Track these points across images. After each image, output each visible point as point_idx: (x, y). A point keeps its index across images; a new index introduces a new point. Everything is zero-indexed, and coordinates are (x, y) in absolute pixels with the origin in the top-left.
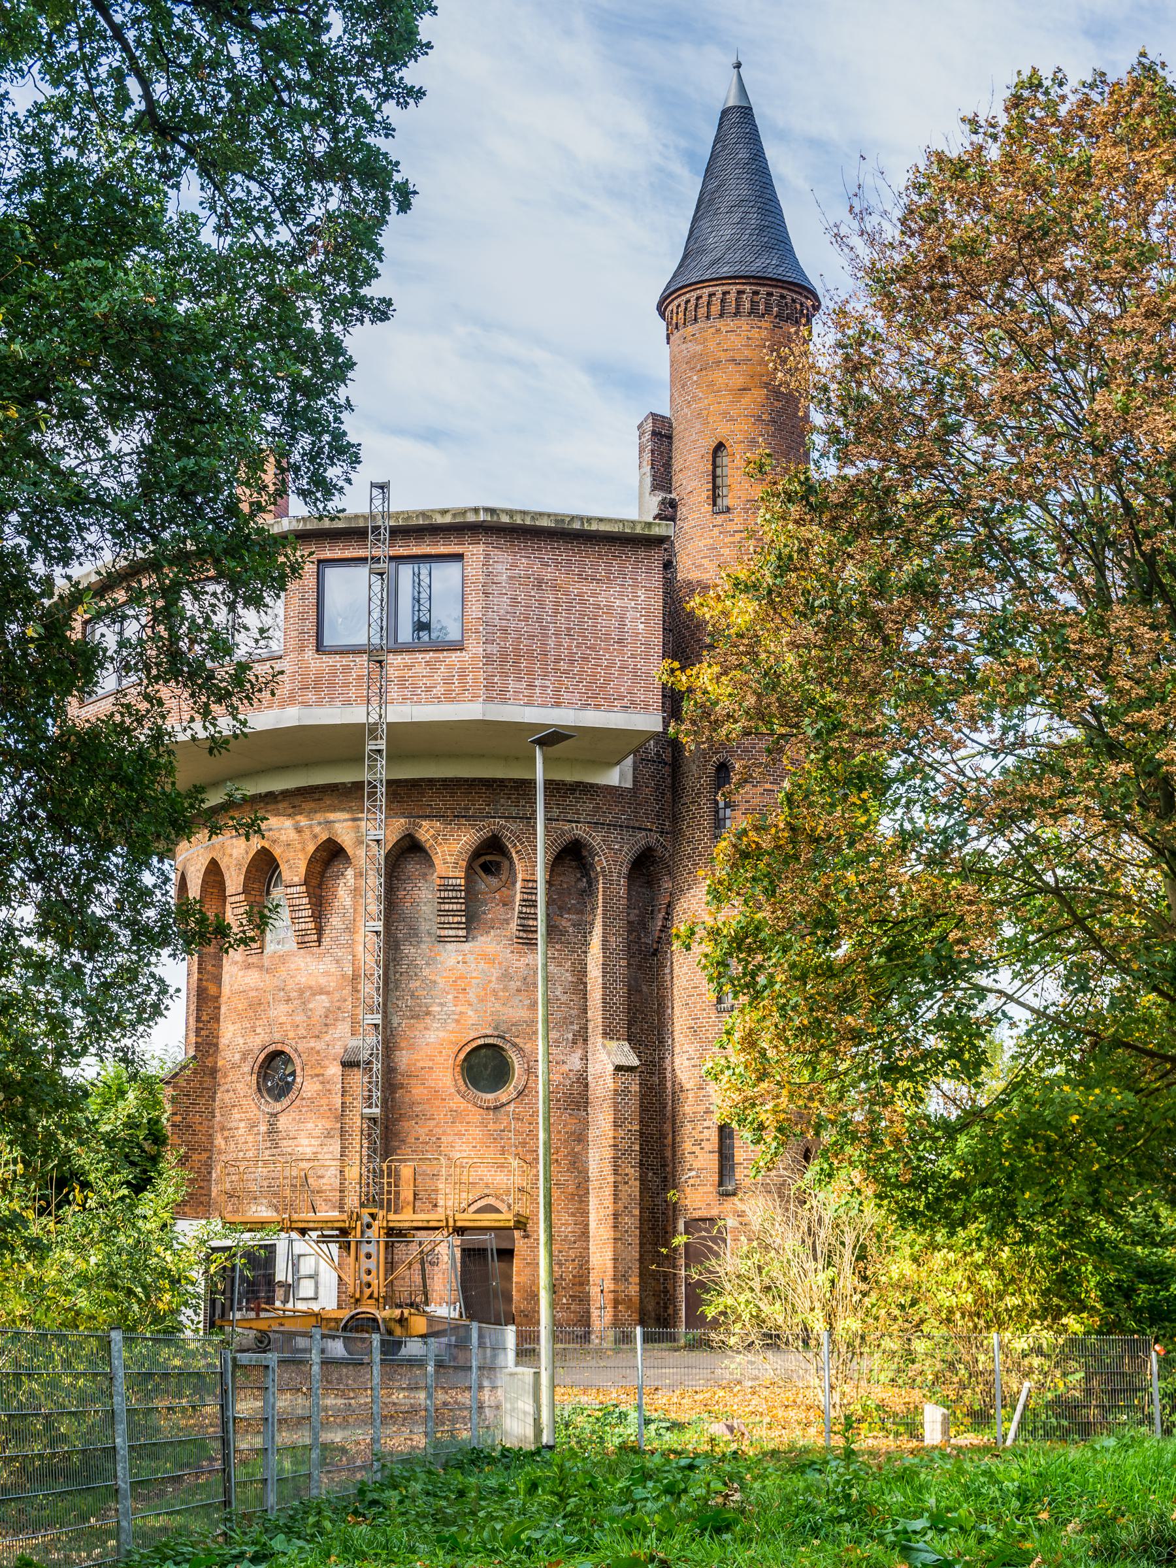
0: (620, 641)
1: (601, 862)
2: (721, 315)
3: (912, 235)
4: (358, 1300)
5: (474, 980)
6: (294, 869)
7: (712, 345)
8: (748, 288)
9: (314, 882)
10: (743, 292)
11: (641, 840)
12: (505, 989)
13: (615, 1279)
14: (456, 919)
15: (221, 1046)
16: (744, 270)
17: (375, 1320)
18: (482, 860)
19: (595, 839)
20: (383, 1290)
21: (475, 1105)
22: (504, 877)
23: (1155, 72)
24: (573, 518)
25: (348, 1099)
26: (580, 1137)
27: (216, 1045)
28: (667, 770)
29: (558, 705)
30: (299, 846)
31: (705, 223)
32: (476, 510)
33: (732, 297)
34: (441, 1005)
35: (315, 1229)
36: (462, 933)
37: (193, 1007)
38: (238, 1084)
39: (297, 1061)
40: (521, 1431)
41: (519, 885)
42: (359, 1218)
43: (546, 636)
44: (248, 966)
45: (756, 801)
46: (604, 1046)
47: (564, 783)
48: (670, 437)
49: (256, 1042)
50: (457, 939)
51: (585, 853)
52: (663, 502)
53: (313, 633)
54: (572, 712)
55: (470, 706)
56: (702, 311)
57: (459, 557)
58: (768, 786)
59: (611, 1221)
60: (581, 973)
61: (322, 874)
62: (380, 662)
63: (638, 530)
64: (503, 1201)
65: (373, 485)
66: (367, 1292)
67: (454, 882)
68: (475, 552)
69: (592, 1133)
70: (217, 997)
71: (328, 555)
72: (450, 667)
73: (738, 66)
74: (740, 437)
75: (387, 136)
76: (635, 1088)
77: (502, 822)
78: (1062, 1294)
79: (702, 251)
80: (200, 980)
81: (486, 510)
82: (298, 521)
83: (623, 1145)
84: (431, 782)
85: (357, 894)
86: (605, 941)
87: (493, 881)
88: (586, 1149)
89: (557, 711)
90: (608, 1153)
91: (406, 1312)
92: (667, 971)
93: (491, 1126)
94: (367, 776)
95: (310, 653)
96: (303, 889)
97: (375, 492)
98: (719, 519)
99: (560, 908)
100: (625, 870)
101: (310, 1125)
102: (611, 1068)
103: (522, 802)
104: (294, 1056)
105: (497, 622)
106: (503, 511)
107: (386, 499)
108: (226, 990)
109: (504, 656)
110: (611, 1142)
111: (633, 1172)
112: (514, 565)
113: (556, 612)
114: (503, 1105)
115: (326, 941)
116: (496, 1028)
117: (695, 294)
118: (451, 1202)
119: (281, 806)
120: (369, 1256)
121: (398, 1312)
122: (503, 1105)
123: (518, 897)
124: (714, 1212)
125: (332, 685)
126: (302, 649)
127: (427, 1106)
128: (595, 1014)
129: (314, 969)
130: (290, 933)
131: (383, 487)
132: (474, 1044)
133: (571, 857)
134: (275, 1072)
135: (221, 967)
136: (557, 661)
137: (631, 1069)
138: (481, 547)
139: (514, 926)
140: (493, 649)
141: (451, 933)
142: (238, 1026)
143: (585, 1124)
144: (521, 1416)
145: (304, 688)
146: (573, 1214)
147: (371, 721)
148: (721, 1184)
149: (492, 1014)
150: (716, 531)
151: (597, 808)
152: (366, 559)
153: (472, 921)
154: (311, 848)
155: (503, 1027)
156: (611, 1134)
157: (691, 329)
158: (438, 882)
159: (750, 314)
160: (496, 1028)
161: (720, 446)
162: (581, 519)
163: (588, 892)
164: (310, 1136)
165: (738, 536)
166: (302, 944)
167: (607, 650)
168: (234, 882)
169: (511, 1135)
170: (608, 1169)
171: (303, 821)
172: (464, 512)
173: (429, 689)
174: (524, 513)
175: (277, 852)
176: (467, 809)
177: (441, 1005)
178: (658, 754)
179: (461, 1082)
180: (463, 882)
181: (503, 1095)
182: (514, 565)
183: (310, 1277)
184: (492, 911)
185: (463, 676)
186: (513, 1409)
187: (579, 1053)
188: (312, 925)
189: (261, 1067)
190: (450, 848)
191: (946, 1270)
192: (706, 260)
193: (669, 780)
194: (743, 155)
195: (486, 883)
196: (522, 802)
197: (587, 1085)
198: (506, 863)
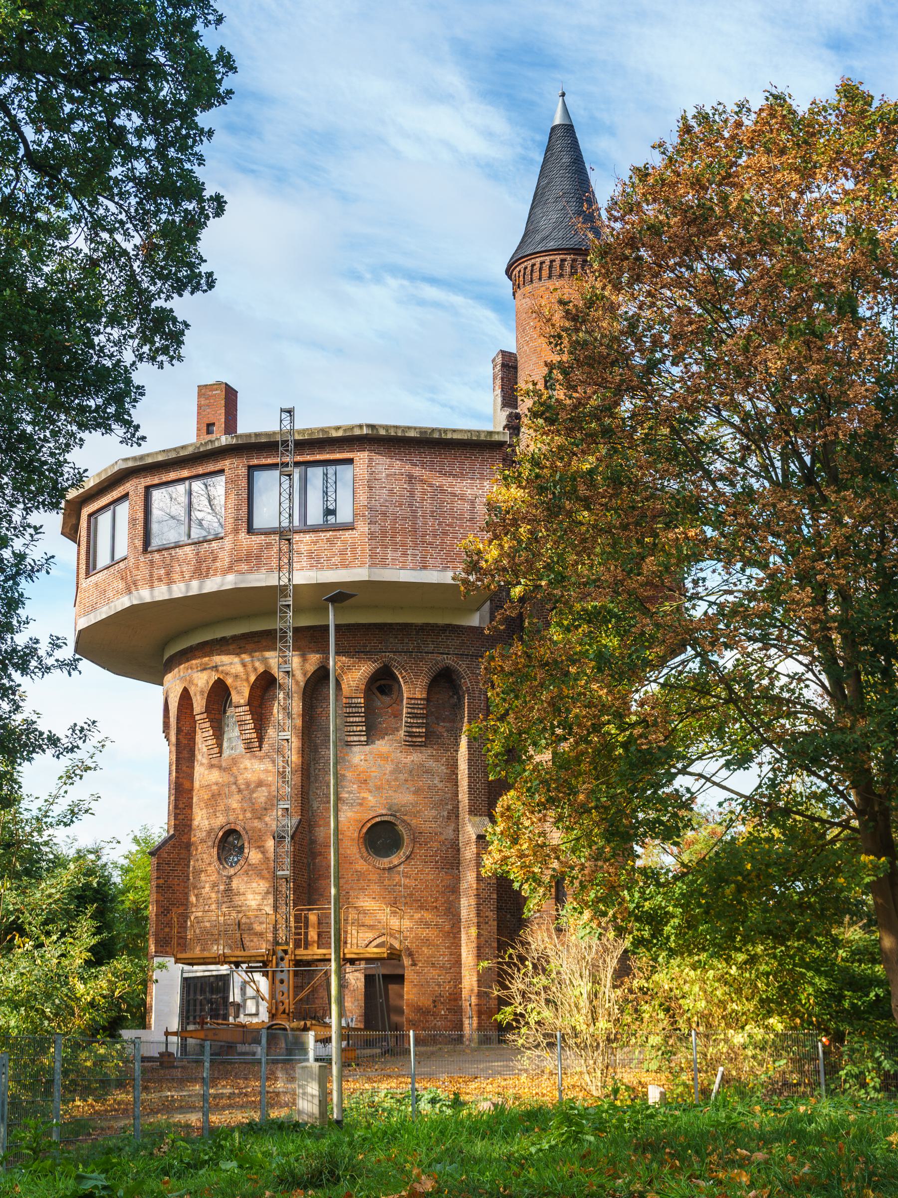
2: (550, 277)
3: (616, 220)
6: (240, 695)
8: (568, 257)
9: (256, 703)
10: (565, 260)
12: (396, 779)
14: (359, 728)
15: (194, 827)
20: (292, 1007)
21: (374, 866)
22: (394, 697)
23: (785, 101)
24: (433, 430)
26: (454, 890)
27: (190, 826)
29: (425, 568)
30: (244, 677)
31: (538, 210)
32: (361, 426)
33: (557, 264)
34: (349, 792)
35: (244, 962)
36: (364, 738)
37: (173, 798)
38: (205, 856)
39: (245, 837)
40: (310, 1110)
41: (405, 701)
42: (274, 953)
43: (415, 517)
44: (212, 766)
46: (470, 821)
48: (515, 368)
49: (220, 820)
51: (454, 677)
52: (510, 416)
53: (245, 519)
54: (435, 573)
55: (359, 570)
56: (536, 275)
57: (350, 461)
60: (453, 766)
61: (262, 697)
62: (289, 540)
63: (483, 438)
64: (396, 938)
65: (282, 410)
66: (281, 1008)
67: (356, 701)
68: (361, 457)
69: (464, 886)
70: (192, 790)
71: (255, 462)
72: (344, 542)
73: (563, 95)
75: (199, 165)
77: (391, 655)
78: (782, 1000)
79: (536, 231)
80: (177, 777)
81: (368, 426)
83: (484, 895)
87: (386, 699)
88: (458, 899)
89: (424, 572)
90: (473, 901)
93: (386, 882)
94: (279, 625)
95: (243, 535)
96: (247, 708)
97: (284, 415)
99: (437, 718)
101: (254, 885)
102: (474, 837)
103: (406, 640)
104: (243, 832)
105: (378, 508)
106: (381, 426)
107: (292, 421)
108: (197, 785)
109: (384, 533)
111: (492, 915)
112: (391, 466)
113: (423, 499)
114: (395, 866)
115: (265, 746)
116: (389, 809)
117: (530, 262)
118: (360, 941)
119: (231, 647)
125: (258, 557)
126: (236, 531)
128: (464, 796)
129: (256, 768)
130: (240, 742)
131: (290, 412)
132: (373, 822)
133: (444, 682)
134: (229, 843)
135: (193, 768)
136: (424, 536)
138: (366, 453)
139: (402, 733)
140: (376, 528)
141: (356, 738)
142: (204, 811)
143: (458, 879)
144: (310, 1098)
145: (239, 560)
146: (449, 948)
147: (282, 583)
149: (386, 798)
152: (277, 465)
153: (372, 732)
154: (253, 678)
155: (395, 808)
156: (475, 886)
157: (528, 288)
158: (344, 700)
160: (389, 809)
162: (440, 430)
164: (254, 893)
166: (249, 749)
167: (461, 526)
168: (199, 704)
169: (401, 889)
170: (473, 915)
171: (246, 657)
172: (352, 428)
174: (396, 427)
175: (229, 681)
177: (349, 792)
179: (364, 850)
181: (395, 860)
184: (385, 722)
185: (354, 549)
186: (304, 1094)
187: (453, 826)
188: (254, 735)
189: (220, 841)
190: (354, 676)
191: (691, 982)
192: (538, 237)
194: (566, 160)
195: (381, 701)
196: (406, 640)
197: (459, 850)
198: (396, 686)
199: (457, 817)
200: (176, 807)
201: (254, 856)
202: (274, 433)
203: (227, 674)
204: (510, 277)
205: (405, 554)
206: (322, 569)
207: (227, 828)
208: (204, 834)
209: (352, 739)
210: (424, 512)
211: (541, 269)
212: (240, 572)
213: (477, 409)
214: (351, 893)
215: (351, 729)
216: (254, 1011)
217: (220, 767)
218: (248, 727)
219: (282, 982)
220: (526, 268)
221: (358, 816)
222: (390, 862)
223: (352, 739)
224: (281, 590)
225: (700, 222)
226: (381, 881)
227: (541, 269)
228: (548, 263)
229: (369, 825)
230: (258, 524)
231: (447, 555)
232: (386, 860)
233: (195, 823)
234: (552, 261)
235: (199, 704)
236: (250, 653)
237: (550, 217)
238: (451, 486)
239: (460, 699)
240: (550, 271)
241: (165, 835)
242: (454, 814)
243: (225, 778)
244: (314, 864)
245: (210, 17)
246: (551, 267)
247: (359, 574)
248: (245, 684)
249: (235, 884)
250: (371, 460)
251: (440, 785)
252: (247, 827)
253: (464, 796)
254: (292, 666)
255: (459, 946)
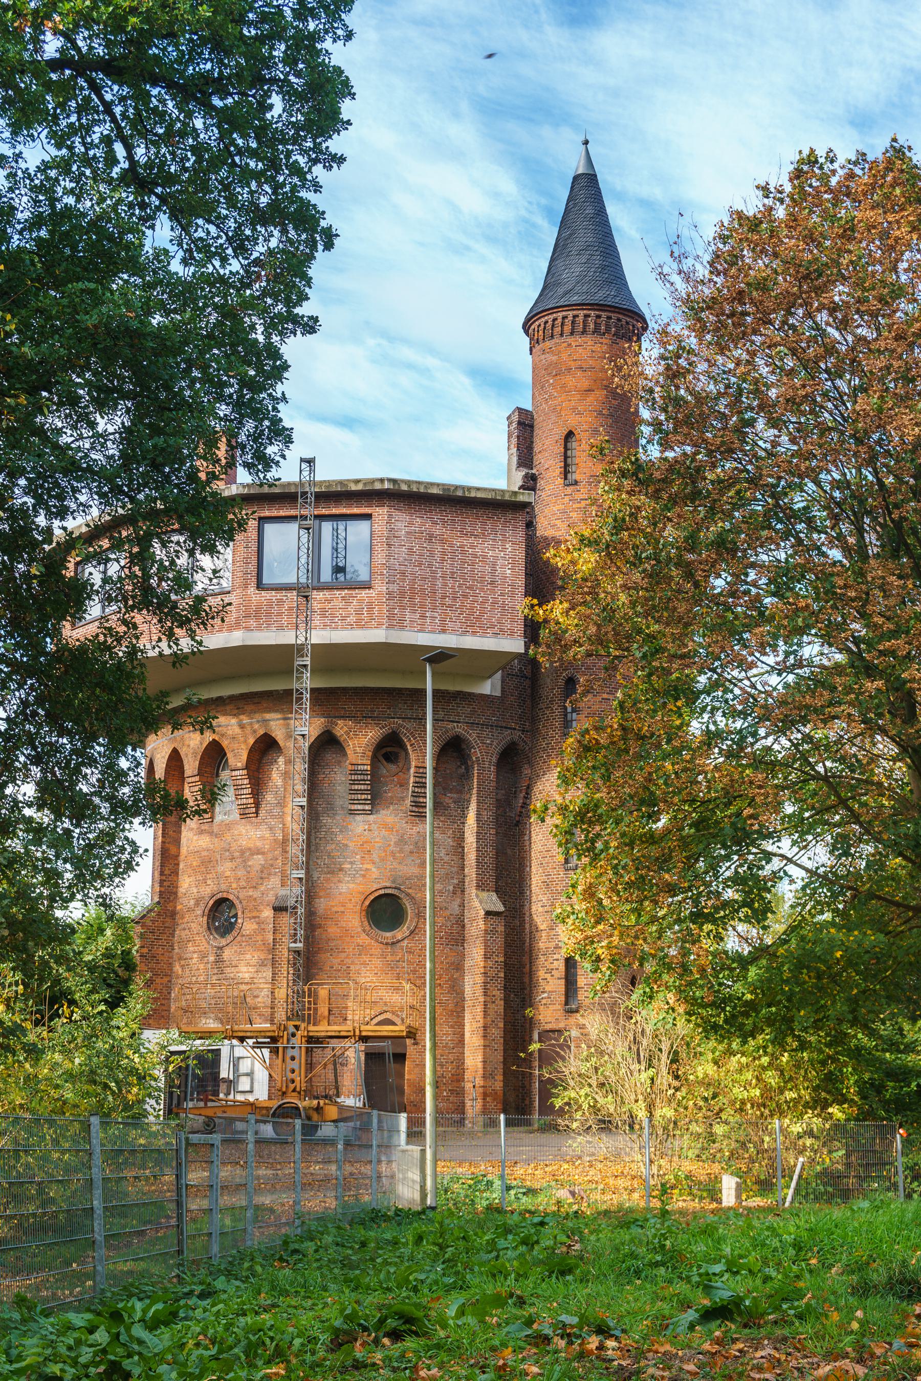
0: (492, 583)
1: (476, 753)
2: (572, 333)
3: (718, 275)
4: (284, 1093)
5: (377, 844)
6: (238, 756)
7: (564, 356)
10: (589, 316)
11: (508, 736)
12: (401, 851)
13: (484, 1077)
14: (363, 797)
15: (179, 894)
16: (590, 299)
17: (297, 1108)
18: (384, 751)
19: (472, 736)
20: (304, 1085)
21: (377, 941)
22: (401, 765)
23: (904, 153)
24: (457, 487)
25: (279, 936)
26: (459, 967)
27: (176, 893)
28: (527, 683)
29: (444, 631)
31: (560, 263)
32: (382, 481)
33: (580, 319)
34: (351, 863)
37: (158, 864)
39: (239, 906)
41: (412, 770)
42: (285, 1028)
44: (201, 832)
45: (596, 707)
46: (477, 896)
47: (447, 692)
48: (532, 426)
49: (207, 891)
50: (364, 812)
51: (464, 746)
52: (526, 476)
54: (454, 637)
56: (558, 330)
57: (368, 517)
58: (605, 696)
59: (481, 1032)
60: (460, 839)
61: (260, 761)
62: (306, 597)
63: (507, 498)
64: (398, 1016)
65: (302, 460)
66: (292, 1086)
67: (362, 767)
68: (380, 512)
69: (468, 964)
70: (177, 856)
72: (361, 601)
73: (586, 143)
74: (585, 427)
75: (315, 191)
76: (501, 929)
77: (400, 721)
78: (828, 1090)
79: (558, 284)
81: (390, 480)
82: (244, 487)
83: (491, 973)
84: (345, 690)
85: (287, 777)
86: (478, 815)
87: (393, 767)
90: (479, 979)
91: (322, 1102)
92: (526, 838)
93: (389, 958)
94: (295, 686)
95: (252, 590)
96: (245, 772)
97: (304, 465)
98: (569, 490)
99: (444, 789)
100: (494, 760)
101: (248, 956)
102: (482, 913)
104: (236, 902)
105: (397, 567)
106: (403, 481)
107: (312, 470)
108: (184, 850)
109: (402, 594)
110: (482, 970)
111: (499, 994)
113: (443, 560)
114: (399, 941)
115: (262, 813)
116: (394, 882)
117: (551, 317)
118: (357, 1017)
119: (228, 708)
120: (293, 1058)
121: (315, 1102)
122: (399, 941)
123: (412, 780)
124: (561, 1025)
125: (269, 614)
127: (339, 942)
128: (471, 871)
129: (251, 835)
131: (310, 462)
132: (377, 894)
133: (452, 750)
134: (221, 914)
135: (180, 832)
136: (444, 597)
137: (497, 914)
139: (408, 802)
140: (394, 588)
141: (360, 807)
143: (463, 956)
144: (410, 1184)
146: (452, 1027)
147: (299, 642)
148: (566, 1003)
150: (567, 499)
151: (474, 711)
153: (376, 798)
154: (251, 741)
155: (399, 881)
156: (482, 964)
157: (548, 344)
158: (350, 767)
159: (594, 333)
160: (394, 882)
161: (570, 435)
163: (466, 776)
164: (248, 965)
165: (583, 503)
167: (482, 589)
168: (191, 766)
169: (405, 964)
170: (479, 992)
171: (246, 720)
172: (373, 481)
173: (343, 619)
174: (419, 483)
175: (225, 743)
176: (372, 711)
177: (351, 863)
178: (520, 670)
179: (366, 923)
180: (369, 768)
181: (399, 934)
182: (411, 523)
183: (247, 1075)
184: (391, 790)
185: (370, 609)
186: (404, 1178)
188: (251, 801)
189: (210, 910)
190: (359, 742)
191: (740, 1071)
193: (529, 691)
194: (590, 211)
195: (387, 769)
198: (403, 753)
199: (463, 891)
200: (162, 873)
201: (248, 926)
202: (294, 484)
203: (223, 735)
204: (526, 332)
205: (423, 617)
206: (336, 628)
207: (219, 896)
208: (192, 902)
209: (356, 807)
210: (444, 573)
211: (563, 324)
212: (248, 629)
213: (488, 466)
214: (352, 967)
215: (356, 797)
216: (248, 1088)
217: (211, 833)
218: (245, 791)
219: (293, 1058)
220: (546, 322)
221: (361, 888)
222: (393, 937)
223: (356, 807)
224: (299, 649)
225: (813, 280)
226: (384, 956)
227: (563, 324)
228: (570, 318)
229: (372, 897)
230: (266, 580)
231: (467, 619)
232: (388, 934)
233: (182, 890)
234: (575, 317)
235: (191, 766)
236: (250, 714)
237: (573, 271)
238: (472, 547)
239: (468, 770)
240: (573, 327)
241: (148, 903)
242: (460, 889)
243: (217, 844)
244: (313, 936)
245: (340, 32)
246: (573, 322)
247: (376, 635)
248: (243, 746)
249: (227, 954)
250: (390, 516)
251: (446, 858)
252: (241, 896)
253: (471, 871)
254: (300, 728)
255: (462, 1026)
